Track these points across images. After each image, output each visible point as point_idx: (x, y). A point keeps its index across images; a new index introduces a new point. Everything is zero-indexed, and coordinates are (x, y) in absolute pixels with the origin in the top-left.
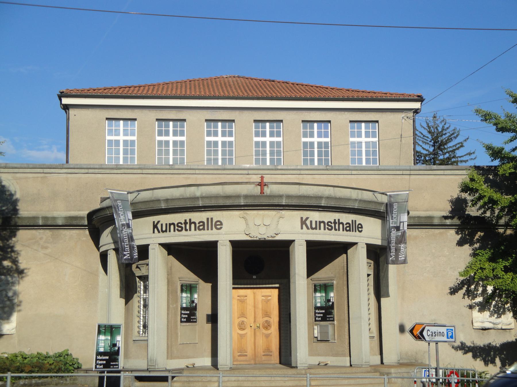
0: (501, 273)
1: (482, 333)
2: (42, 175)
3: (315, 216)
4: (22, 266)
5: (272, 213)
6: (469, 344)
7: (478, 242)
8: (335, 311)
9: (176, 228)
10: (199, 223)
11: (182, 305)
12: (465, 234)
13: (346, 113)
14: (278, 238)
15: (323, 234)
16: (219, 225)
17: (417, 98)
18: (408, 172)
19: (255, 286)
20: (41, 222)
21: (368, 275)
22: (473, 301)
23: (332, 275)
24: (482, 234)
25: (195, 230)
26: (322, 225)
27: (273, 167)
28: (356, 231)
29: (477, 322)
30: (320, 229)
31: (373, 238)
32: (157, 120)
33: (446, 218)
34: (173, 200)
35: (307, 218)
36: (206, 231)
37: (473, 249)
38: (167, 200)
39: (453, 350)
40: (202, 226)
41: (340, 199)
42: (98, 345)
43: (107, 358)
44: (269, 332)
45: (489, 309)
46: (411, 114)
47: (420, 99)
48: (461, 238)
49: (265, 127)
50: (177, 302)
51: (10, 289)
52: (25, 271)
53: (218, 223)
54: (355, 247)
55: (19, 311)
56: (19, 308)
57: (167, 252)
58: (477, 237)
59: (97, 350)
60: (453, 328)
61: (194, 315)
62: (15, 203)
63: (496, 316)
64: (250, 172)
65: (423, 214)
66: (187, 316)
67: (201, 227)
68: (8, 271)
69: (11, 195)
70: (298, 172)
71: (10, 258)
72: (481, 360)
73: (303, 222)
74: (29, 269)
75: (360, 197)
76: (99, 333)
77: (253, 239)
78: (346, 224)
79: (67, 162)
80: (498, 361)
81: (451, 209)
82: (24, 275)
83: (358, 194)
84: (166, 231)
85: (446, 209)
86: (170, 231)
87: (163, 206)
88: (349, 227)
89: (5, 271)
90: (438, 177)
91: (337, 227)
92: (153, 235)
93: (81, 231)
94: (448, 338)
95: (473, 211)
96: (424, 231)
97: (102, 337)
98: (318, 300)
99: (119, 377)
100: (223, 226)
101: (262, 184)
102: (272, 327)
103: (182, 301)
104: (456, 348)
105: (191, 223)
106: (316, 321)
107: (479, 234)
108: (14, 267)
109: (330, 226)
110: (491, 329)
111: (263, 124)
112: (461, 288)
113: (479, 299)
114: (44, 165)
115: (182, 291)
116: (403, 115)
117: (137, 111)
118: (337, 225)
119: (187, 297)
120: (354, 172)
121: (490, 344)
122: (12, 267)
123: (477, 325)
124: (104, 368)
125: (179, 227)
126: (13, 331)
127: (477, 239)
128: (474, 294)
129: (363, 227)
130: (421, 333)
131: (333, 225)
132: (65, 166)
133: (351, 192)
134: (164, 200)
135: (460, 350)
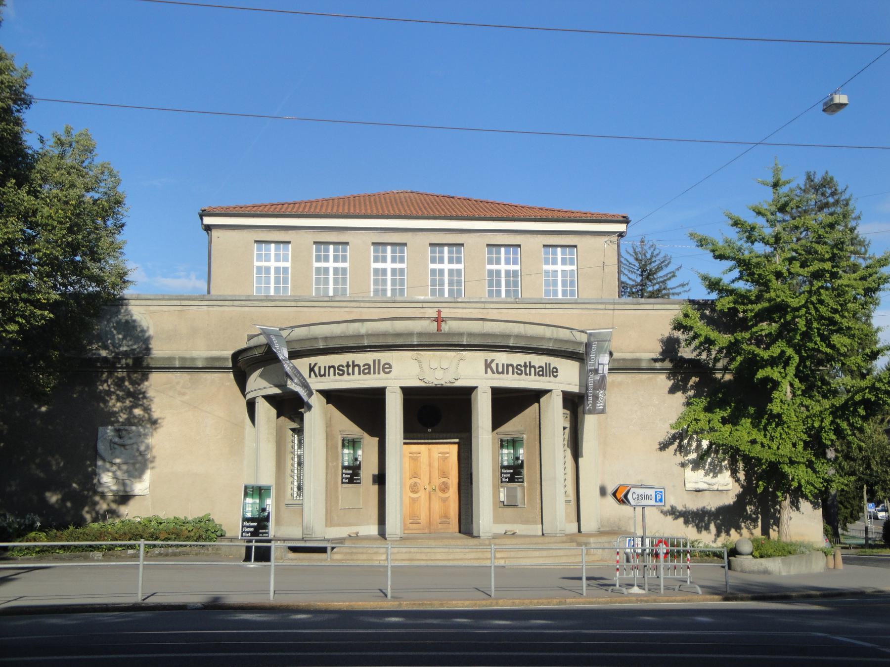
0: (717, 425)
1: (696, 496)
3: (502, 358)
5: (451, 354)
6: (680, 508)
8: (525, 471)
9: (337, 371)
10: (364, 365)
11: (343, 463)
12: (677, 379)
13: (539, 236)
14: (458, 384)
16: (387, 368)
17: (622, 219)
18: (611, 306)
19: (430, 441)
20: (177, 364)
23: (522, 428)
24: (697, 379)
25: (359, 374)
26: (510, 368)
28: (550, 376)
29: (690, 482)
30: (507, 373)
33: (655, 360)
34: (333, 338)
35: (492, 361)
36: (372, 376)
37: (687, 398)
38: (326, 339)
39: (662, 515)
40: (367, 369)
41: (532, 338)
42: (244, 509)
43: (255, 524)
44: (446, 495)
45: (704, 468)
46: (615, 238)
47: (625, 220)
48: (673, 384)
50: (337, 459)
51: (142, 442)
52: (159, 421)
58: (691, 383)
60: (663, 490)
62: (147, 341)
63: (711, 475)
65: (628, 356)
67: (366, 371)
68: (140, 422)
69: (143, 331)
70: (482, 305)
71: (141, 405)
72: (693, 527)
73: (488, 365)
75: (555, 336)
76: (246, 495)
77: (428, 385)
79: (209, 292)
80: (712, 527)
81: (661, 350)
82: (157, 426)
84: (324, 375)
85: (656, 350)
86: (329, 375)
87: (321, 345)
88: (542, 371)
90: (646, 312)
93: (225, 375)
94: (656, 501)
95: (687, 353)
97: (249, 500)
99: (269, 548)
100: (393, 370)
101: (439, 320)
103: (343, 459)
107: (694, 380)
108: (146, 415)
109: (519, 370)
110: (705, 490)
111: (441, 248)
112: (672, 443)
115: (343, 446)
117: (290, 232)
119: (349, 454)
121: (704, 508)
122: (144, 416)
123: (690, 486)
125: (340, 371)
126: (147, 492)
127: (691, 385)
128: (687, 450)
130: (626, 496)
131: (345, 369)
133: (544, 329)
135: (670, 515)
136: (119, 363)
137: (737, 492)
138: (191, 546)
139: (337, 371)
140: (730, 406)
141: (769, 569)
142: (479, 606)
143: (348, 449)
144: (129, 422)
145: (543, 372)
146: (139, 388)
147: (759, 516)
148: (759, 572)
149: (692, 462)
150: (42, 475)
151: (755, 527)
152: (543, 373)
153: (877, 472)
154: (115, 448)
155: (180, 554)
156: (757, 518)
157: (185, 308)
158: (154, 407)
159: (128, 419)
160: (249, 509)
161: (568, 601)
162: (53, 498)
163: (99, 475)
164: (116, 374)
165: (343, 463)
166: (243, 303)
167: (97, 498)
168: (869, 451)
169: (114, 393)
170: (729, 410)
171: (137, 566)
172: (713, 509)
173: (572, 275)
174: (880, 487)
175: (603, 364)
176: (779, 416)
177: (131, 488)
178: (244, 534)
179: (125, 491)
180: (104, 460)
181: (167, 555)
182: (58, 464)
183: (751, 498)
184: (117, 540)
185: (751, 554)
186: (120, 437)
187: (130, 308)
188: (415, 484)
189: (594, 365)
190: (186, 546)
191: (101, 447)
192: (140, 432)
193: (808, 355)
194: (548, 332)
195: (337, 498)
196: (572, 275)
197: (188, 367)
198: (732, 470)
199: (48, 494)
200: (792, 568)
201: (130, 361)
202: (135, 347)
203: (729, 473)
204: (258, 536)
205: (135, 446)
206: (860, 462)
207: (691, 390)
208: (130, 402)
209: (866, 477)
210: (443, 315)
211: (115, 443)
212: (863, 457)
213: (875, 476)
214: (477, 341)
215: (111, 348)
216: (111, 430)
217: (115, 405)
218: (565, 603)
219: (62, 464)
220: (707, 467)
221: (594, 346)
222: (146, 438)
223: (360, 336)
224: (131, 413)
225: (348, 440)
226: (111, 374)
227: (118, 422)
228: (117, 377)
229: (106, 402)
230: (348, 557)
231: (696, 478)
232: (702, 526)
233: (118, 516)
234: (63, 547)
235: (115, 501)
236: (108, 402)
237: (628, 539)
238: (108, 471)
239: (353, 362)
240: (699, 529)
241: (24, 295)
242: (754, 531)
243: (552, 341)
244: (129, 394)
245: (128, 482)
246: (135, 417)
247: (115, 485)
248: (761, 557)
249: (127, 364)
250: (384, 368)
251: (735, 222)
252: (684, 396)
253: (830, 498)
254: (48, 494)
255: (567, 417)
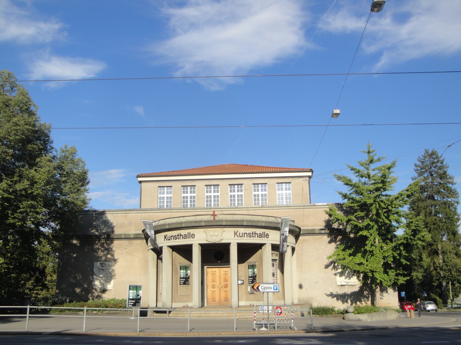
0: (347, 257)
1: (342, 288)
2: (125, 214)
3: (242, 230)
4: (116, 258)
5: (219, 229)
6: (334, 293)
7: (339, 241)
8: (257, 278)
9: (174, 238)
11: (180, 276)
12: (332, 237)
13: (275, 179)
14: (222, 242)
15: (246, 239)
16: (193, 236)
17: (310, 170)
18: (303, 207)
19: (222, 266)
20: (123, 237)
21: (274, 260)
22: (337, 272)
23: (256, 260)
24: (341, 237)
25: (182, 239)
26: (246, 235)
27: (191, 208)
28: (265, 238)
29: (338, 282)
30: (244, 237)
31: (275, 241)
32: (229, 185)
33: (321, 230)
34: (171, 224)
35: (237, 232)
36: (262, 238)
37: (336, 245)
38: (169, 224)
39: (327, 297)
40: (185, 237)
41: (254, 221)
42: (129, 295)
43: (134, 301)
44: (227, 289)
45: (345, 275)
46: (307, 179)
47: (311, 171)
48: (330, 239)
49: (282, 186)
50: (178, 274)
51: (111, 269)
52: (117, 260)
53: (193, 235)
54: (265, 245)
55: (115, 279)
56: (115, 277)
57: (172, 250)
58: (338, 239)
59: (128, 297)
60: (278, 285)
61: (188, 281)
62: (113, 228)
63: (348, 278)
64: (223, 210)
65: (310, 228)
66: (251, 281)
68: (110, 260)
69: (111, 224)
70: (247, 209)
71: (111, 254)
72: (340, 301)
73: (235, 234)
74: (119, 259)
75: (267, 220)
76: (130, 289)
77: (210, 242)
78: (259, 234)
79: (140, 208)
80: (349, 301)
81: (325, 225)
82: (117, 262)
83: (266, 219)
84: (170, 240)
85: (322, 225)
86: (171, 239)
87: (167, 227)
88: (261, 235)
89: (108, 260)
90: (318, 209)
91: (179, 238)
92: (165, 242)
93: (142, 241)
94: (274, 290)
95: (335, 226)
96: (311, 236)
97: (131, 291)
98: (182, 274)
99: (147, 311)
101: (214, 215)
102: (229, 287)
103: (181, 274)
104: (328, 295)
105: (180, 235)
106: (249, 283)
107: (340, 237)
108: (112, 258)
109: (250, 235)
110: (346, 285)
111: (234, 186)
112: (330, 265)
113: (340, 270)
114: (126, 209)
115: (181, 269)
116: (302, 179)
117: (172, 182)
118: (254, 235)
119: (251, 271)
120: (275, 208)
121: (345, 293)
122: (111, 258)
123: (339, 283)
124: (132, 306)
125: (175, 237)
126: (112, 288)
127: (338, 240)
128: (337, 268)
129: (269, 235)
130: (258, 288)
131: (252, 235)
132: (140, 210)
134: (167, 224)
136: (102, 237)
137: (360, 286)
138: (121, 310)
139: (174, 238)
140: (353, 248)
141: (361, 319)
142: (177, 335)
143: (251, 269)
144: (106, 260)
145: (260, 236)
146: (110, 247)
147: (370, 296)
148: (356, 320)
149: (339, 273)
150: (74, 281)
151: (368, 300)
152: (186, 237)
153: (454, 275)
154: (100, 271)
155: (116, 313)
156: (369, 297)
157: (127, 214)
158: (115, 254)
159: (105, 259)
160: (131, 295)
161: (222, 333)
162: (78, 290)
163: (94, 281)
164: (101, 241)
165: (249, 275)
166: (149, 211)
167: (94, 291)
168: (451, 267)
169: (100, 249)
170: (353, 250)
171: (83, 318)
172: (349, 293)
173: (290, 195)
174: (457, 282)
175: (286, 231)
176: (372, 251)
177: (106, 287)
178: (129, 305)
179: (104, 288)
180: (96, 276)
181: (110, 314)
182: (80, 277)
183: (366, 288)
184: (90, 307)
185: (353, 312)
186: (102, 266)
187: (107, 215)
188: (214, 285)
189: (283, 232)
190: (118, 310)
191: (95, 270)
192: (110, 264)
193: (382, 225)
194: (264, 219)
195: (178, 291)
196: (290, 195)
197: (127, 238)
198: (357, 276)
199: (76, 289)
200: (374, 318)
201: (106, 236)
202: (108, 230)
203: (356, 277)
204: (135, 306)
205: (108, 270)
206: (448, 271)
207: (338, 242)
208: (106, 252)
209: (450, 278)
210: (216, 213)
211: (100, 269)
212: (449, 269)
213: (454, 277)
214: (229, 224)
215: (99, 231)
216: (99, 264)
217: (100, 253)
218: (221, 334)
219: (81, 277)
220: (346, 275)
221: (283, 224)
222: (112, 267)
223: (181, 223)
224: (106, 257)
225: (183, 267)
226: (99, 241)
227: (102, 260)
228: (102, 243)
229: (97, 253)
230: (175, 315)
231: (341, 280)
232: (344, 301)
233: (102, 298)
234: (69, 310)
235: (100, 292)
236: (98, 252)
237: (260, 307)
238: (98, 280)
239: (180, 234)
240: (343, 302)
241: (32, 210)
242: (367, 302)
243: (264, 222)
244: (106, 249)
245: (105, 284)
246: (108, 258)
247: (100, 285)
248: (358, 313)
249: (104, 237)
250: (192, 236)
251: (352, 169)
252: (335, 244)
253: (444, 287)
254: (76, 289)
255: (277, 255)
